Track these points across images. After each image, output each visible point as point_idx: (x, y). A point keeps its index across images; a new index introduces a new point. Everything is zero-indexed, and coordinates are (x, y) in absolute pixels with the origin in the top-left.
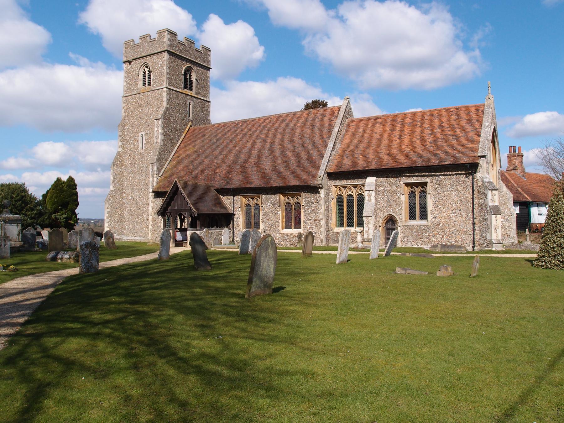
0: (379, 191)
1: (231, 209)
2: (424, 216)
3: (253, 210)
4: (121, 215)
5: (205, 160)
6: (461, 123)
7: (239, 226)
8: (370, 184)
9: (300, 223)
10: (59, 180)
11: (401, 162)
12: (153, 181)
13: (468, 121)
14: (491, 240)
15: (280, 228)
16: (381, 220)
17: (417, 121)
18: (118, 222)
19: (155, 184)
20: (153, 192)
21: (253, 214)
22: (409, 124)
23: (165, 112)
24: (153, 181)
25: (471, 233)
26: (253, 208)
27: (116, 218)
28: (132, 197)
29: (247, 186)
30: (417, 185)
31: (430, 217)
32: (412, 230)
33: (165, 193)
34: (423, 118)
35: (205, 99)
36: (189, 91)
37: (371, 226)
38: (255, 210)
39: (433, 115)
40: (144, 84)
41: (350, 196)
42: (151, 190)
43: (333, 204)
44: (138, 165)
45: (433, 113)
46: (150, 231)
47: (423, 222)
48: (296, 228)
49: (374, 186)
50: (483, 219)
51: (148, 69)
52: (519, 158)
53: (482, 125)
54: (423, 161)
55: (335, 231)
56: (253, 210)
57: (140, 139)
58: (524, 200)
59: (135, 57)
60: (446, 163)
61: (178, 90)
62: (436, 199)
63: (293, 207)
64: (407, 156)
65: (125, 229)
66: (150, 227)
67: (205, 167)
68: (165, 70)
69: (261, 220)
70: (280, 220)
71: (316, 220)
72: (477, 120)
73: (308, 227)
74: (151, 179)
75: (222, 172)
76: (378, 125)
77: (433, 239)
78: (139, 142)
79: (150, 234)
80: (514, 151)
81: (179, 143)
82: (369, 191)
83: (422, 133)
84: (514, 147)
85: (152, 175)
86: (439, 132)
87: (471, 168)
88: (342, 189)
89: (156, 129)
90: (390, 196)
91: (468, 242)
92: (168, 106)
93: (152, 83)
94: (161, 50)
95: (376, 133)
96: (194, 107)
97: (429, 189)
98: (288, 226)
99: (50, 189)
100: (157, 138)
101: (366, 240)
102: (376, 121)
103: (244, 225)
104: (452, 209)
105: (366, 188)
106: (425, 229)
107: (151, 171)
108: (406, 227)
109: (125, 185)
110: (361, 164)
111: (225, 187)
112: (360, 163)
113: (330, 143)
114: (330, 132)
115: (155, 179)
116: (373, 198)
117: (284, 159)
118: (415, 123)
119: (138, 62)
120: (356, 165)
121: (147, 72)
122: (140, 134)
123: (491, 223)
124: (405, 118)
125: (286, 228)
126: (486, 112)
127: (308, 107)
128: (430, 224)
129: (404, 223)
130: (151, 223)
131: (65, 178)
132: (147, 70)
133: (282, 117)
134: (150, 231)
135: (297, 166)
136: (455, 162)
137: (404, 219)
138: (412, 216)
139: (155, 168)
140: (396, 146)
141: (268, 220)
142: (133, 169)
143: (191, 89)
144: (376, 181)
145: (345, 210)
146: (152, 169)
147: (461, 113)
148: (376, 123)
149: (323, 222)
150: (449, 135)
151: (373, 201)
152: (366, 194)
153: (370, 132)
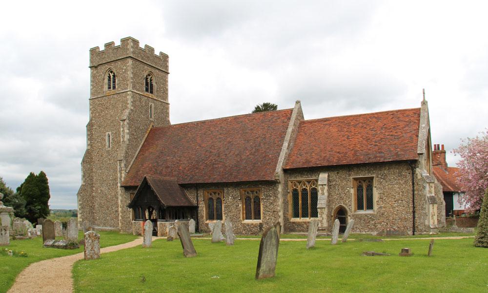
0: (331, 185)
1: (195, 202)
2: (370, 206)
3: (215, 203)
4: (92, 207)
5: (168, 158)
6: (402, 124)
7: (202, 217)
8: (322, 180)
9: (260, 214)
10: (32, 175)
11: (350, 159)
12: (121, 177)
13: (407, 123)
14: (429, 226)
15: (241, 219)
16: (333, 210)
17: (362, 123)
18: (89, 214)
19: (123, 180)
20: (121, 187)
21: (215, 206)
22: (355, 126)
23: (130, 114)
24: (122, 176)
25: (412, 220)
26: (215, 201)
27: (87, 209)
28: (101, 190)
29: (210, 181)
30: (364, 179)
31: (376, 207)
32: (361, 219)
33: (137, 187)
34: (367, 120)
35: (165, 102)
36: (151, 94)
37: (325, 216)
38: (217, 203)
39: (376, 118)
40: (109, 88)
41: (305, 190)
42: (119, 185)
43: (290, 197)
44: (106, 162)
45: (376, 116)
46: (120, 222)
47: (370, 212)
48: (255, 219)
49: (326, 181)
50: (422, 207)
51: (113, 74)
52: (443, 154)
53: (419, 127)
54: (370, 158)
55: (291, 221)
56: (215, 203)
57: (107, 138)
58: (448, 190)
59: (101, 63)
60: (390, 160)
61: (141, 93)
62: (382, 192)
63: (253, 200)
64: (355, 154)
65: (96, 220)
66: (120, 218)
67: (169, 164)
68: (130, 74)
69: (223, 212)
70: (241, 212)
71: (274, 211)
72: (415, 122)
73: (268, 218)
74: (119, 175)
75: (185, 168)
76: (327, 127)
77: (379, 226)
78: (106, 141)
79: (120, 224)
80: (439, 148)
81: (143, 142)
82: (322, 185)
83: (367, 133)
84: (438, 145)
85: (121, 171)
86: (382, 133)
87: (412, 164)
88: (298, 184)
89: (122, 129)
90: (340, 190)
91: (408, 228)
92: (132, 108)
93: (117, 87)
94: (125, 56)
95: (326, 134)
96: (155, 108)
97: (375, 183)
98: (248, 217)
99: (24, 183)
100: (123, 137)
101: (320, 229)
102: (325, 123)
103: (208, 217)
104: (395, 200)
105: (319, 183)
106: (372, 218)
107: (118, 167)
108: (355, 217)
109: (94, 180)
110: (315, 162)
111: (189, 182)
112: (313, 160)
113: (285, 142)
114: (285, 133)
115: (123, 175)
116: (325, 191)
117: (243, 157)
118: (361, 125)
119: (103, 67)
120: (311, 162)
121: (112, 77)
122: (107, 133)
123: (429, 211)
124: (352, 121)
125: (247, 218)
126: (422, 115)
127: (258, 110)
128: (376, 213)
129: (353, 213)
130: (120, 214)
131: (37, 173)
132: (112, 75)
133: (238, 118)
134: (120, 222)
135: (255, 164)
136: (398, 159)
137: (353, 210)
138: (360, 207)
139: (123, 165)
140: (345, 145)
141: (230, 212)
142: (101, 165)
143: (152, 92)
144: (329, 176)
145: (300, 202)
146: (120, 165)
147: (401, 116)
148: (326, 125)
149: (281, 214)
150: (392, 135)
151: (326, 194)
152: (319, 188)
153: (320, 132)
